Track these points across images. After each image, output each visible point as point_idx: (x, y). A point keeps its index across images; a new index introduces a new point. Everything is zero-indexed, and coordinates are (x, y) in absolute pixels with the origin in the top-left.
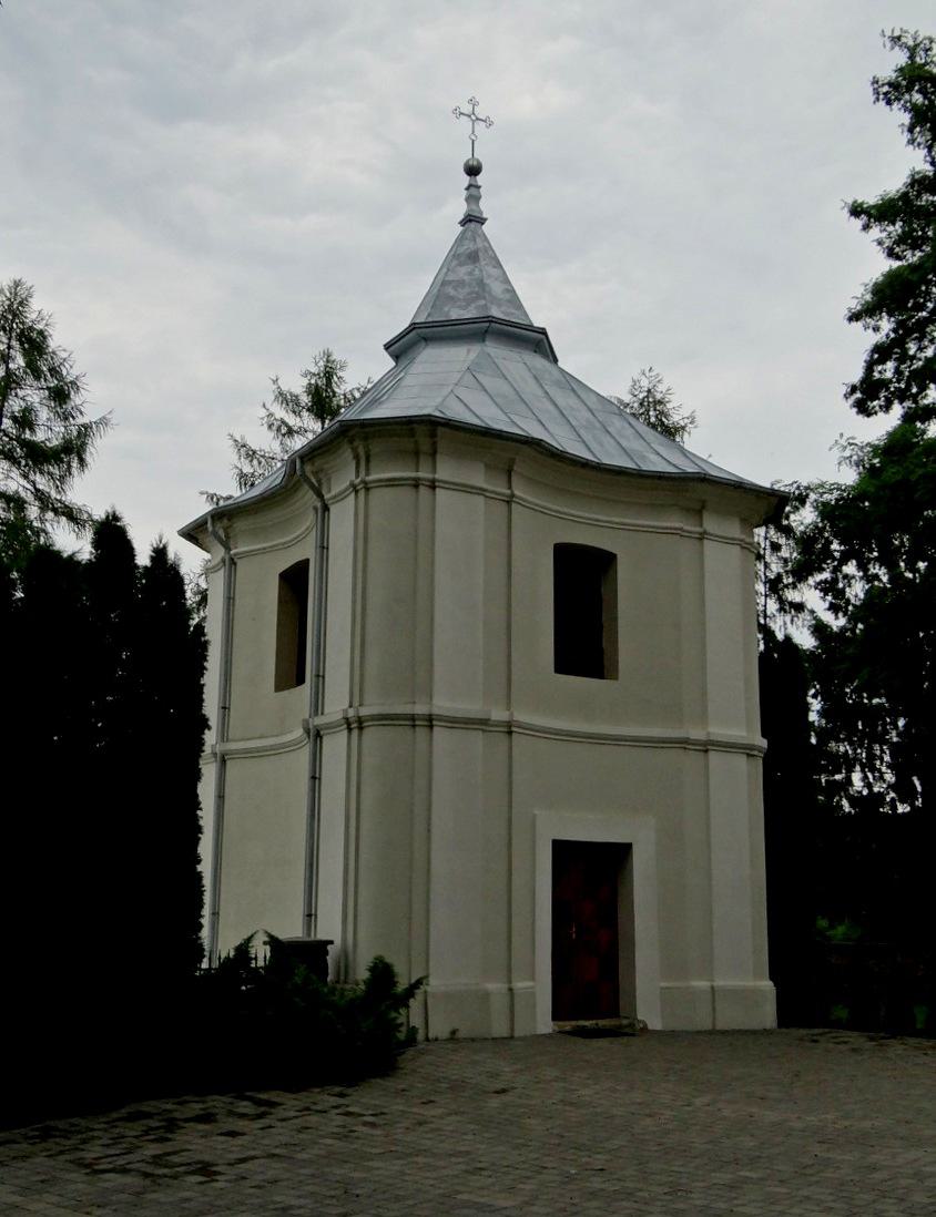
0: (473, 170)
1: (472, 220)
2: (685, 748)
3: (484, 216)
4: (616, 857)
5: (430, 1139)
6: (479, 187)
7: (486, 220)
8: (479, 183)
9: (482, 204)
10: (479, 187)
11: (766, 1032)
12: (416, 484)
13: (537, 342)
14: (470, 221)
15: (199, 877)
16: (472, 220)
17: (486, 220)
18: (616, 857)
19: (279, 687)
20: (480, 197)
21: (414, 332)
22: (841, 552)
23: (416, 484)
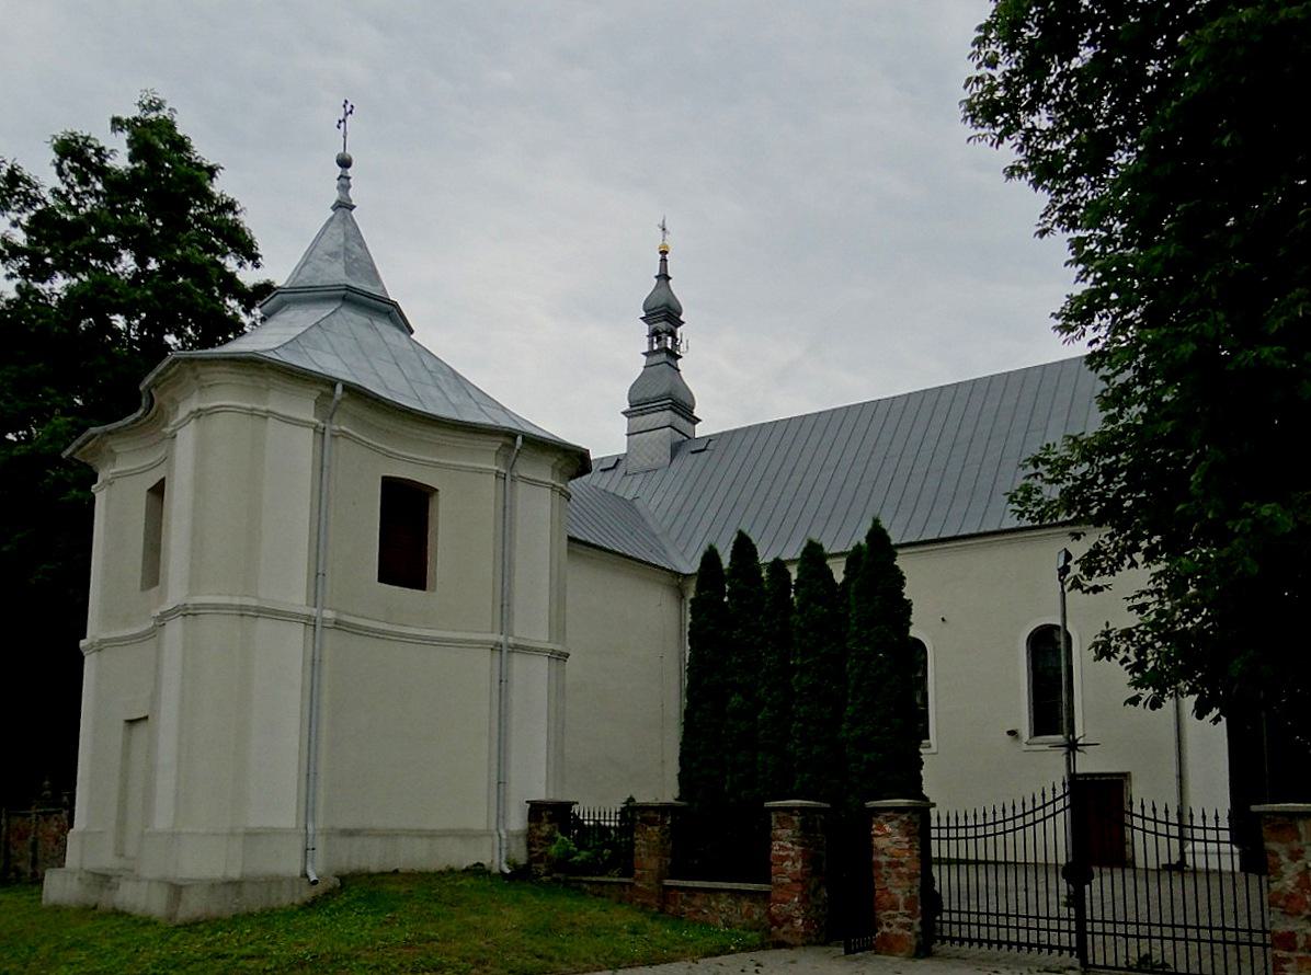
0: (345, 163)
1: (343, 206)
2: (320, 661)
3: (354, 203)
4: (389, 574)
5: (417, 435)
6: (349, 178)
7: (355, 207)
8: (350, 175)
9: (351, 193)
10: (349, 178)
11: (809, 534)
12: (252, 412)
13: (389, 312)
14: (340, 206)
15: (207, 348)
16: (343, 206)
17: (355, 207)
18: (389, 574)
19: (142, 589)
20: (349, 187)
21: (278, 296)
22: (1142, 315)
23: (252, 412)
